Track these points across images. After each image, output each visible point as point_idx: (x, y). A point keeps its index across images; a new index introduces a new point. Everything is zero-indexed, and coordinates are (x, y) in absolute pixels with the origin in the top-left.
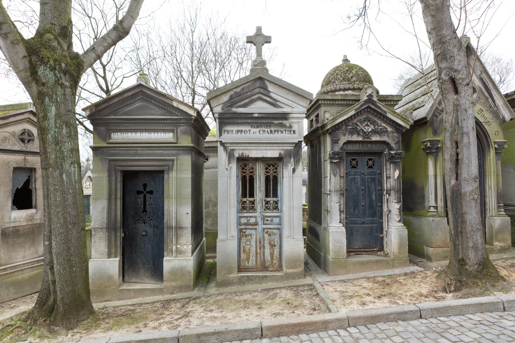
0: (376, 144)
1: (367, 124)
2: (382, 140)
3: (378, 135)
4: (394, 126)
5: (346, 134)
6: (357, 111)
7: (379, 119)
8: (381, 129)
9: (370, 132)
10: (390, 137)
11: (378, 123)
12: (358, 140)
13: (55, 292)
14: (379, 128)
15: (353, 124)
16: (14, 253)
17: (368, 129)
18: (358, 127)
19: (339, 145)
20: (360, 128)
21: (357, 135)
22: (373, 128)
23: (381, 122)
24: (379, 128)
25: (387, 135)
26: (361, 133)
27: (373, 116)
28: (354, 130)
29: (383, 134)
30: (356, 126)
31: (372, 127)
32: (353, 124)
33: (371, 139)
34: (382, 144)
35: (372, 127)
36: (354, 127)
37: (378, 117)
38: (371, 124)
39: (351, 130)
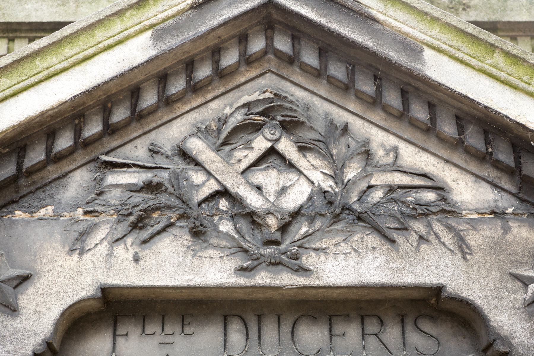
0: (372, 327)
1: (272, 152)
2: (409, 279)
3: (373, 240)
4: (497, 165)
5: (84, 234)
6: (172, 42)
7: (377, 117)
8: (391, 189)
9: (296, 214)
10: (478, 256)
11: (367, 142)
12: (197, 280)
13: (285, 265)
14: (378, 179)
15: (154, 152)
16: (502, 60)
17: (283, 190)
18: (198, 177)
19: (17, 323)
20: (212, 186)
21: (186, 239)
22: (327, 185)
23: (392, 141)
24: (378, 179)
25: (447, 238)
26: (226, 227)
27: (323, 89)
28: (163, 199)
29: (419, 226)
30: (179, 164)
31: (317, 177)
32: (154, 152)
33: (303, 270)
34: (427, 326)
35: (317, 177)
36: (163, 176)
37: (360, 97)
38: (302, 149)
39: (137, 198)
